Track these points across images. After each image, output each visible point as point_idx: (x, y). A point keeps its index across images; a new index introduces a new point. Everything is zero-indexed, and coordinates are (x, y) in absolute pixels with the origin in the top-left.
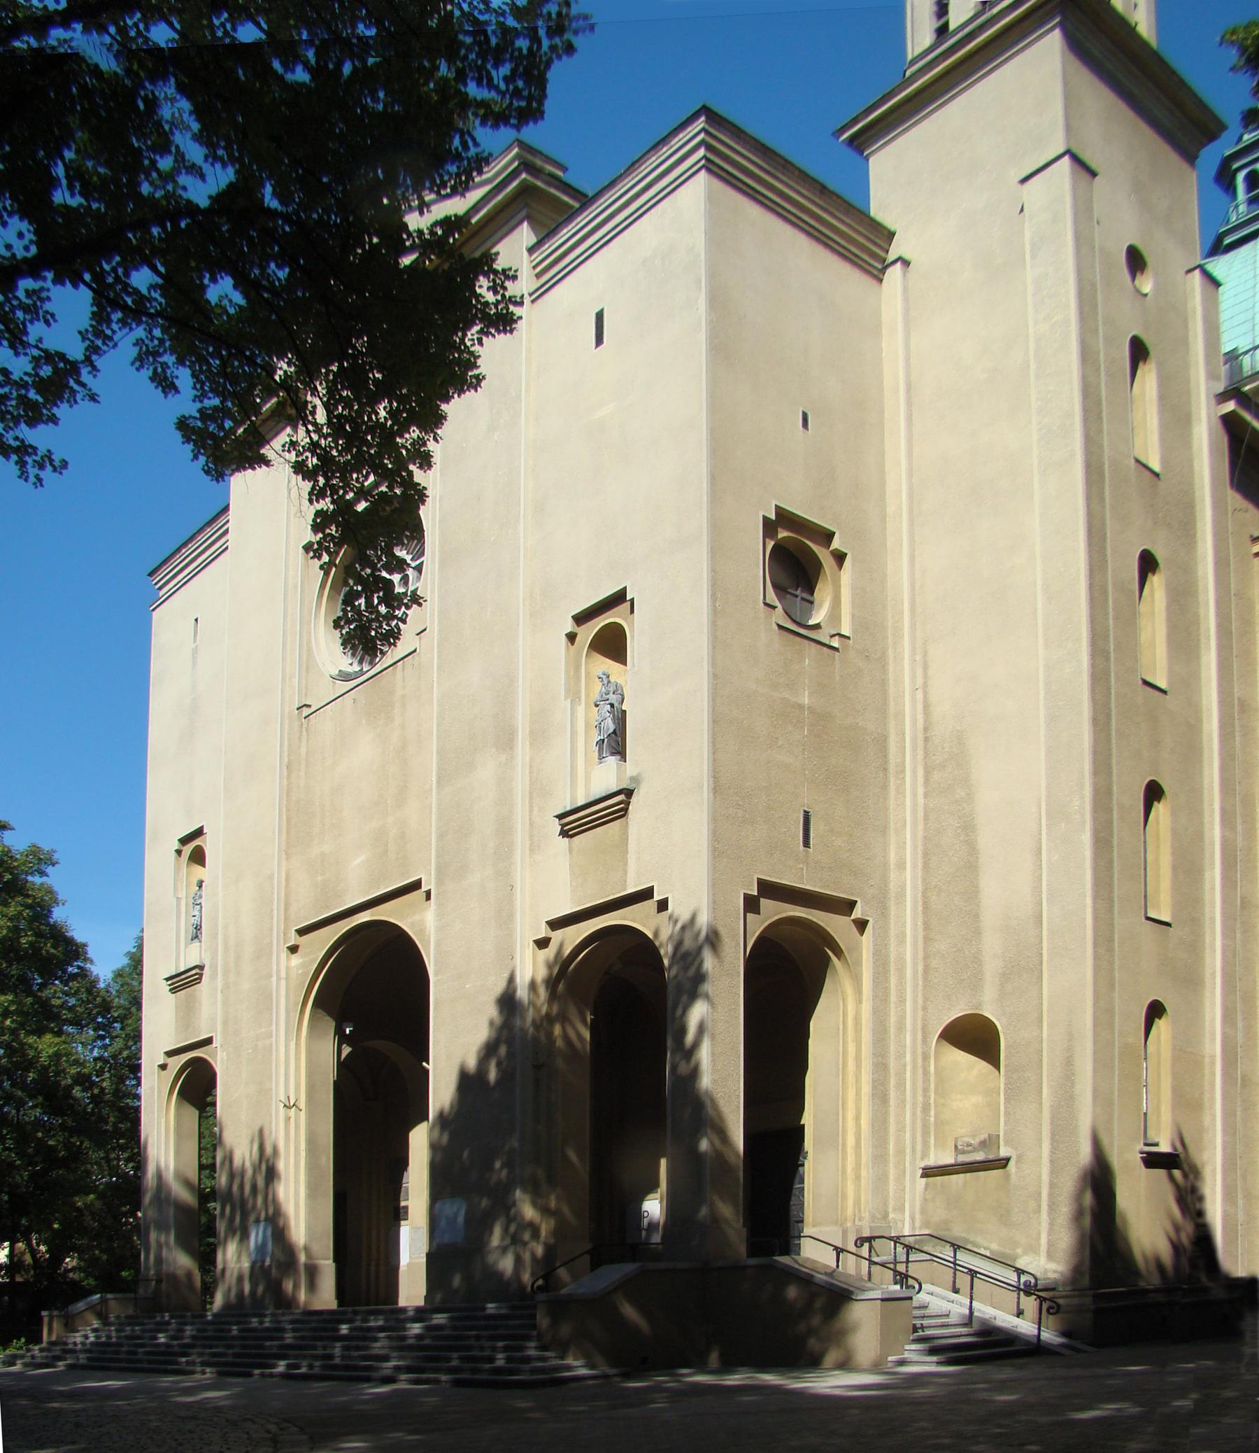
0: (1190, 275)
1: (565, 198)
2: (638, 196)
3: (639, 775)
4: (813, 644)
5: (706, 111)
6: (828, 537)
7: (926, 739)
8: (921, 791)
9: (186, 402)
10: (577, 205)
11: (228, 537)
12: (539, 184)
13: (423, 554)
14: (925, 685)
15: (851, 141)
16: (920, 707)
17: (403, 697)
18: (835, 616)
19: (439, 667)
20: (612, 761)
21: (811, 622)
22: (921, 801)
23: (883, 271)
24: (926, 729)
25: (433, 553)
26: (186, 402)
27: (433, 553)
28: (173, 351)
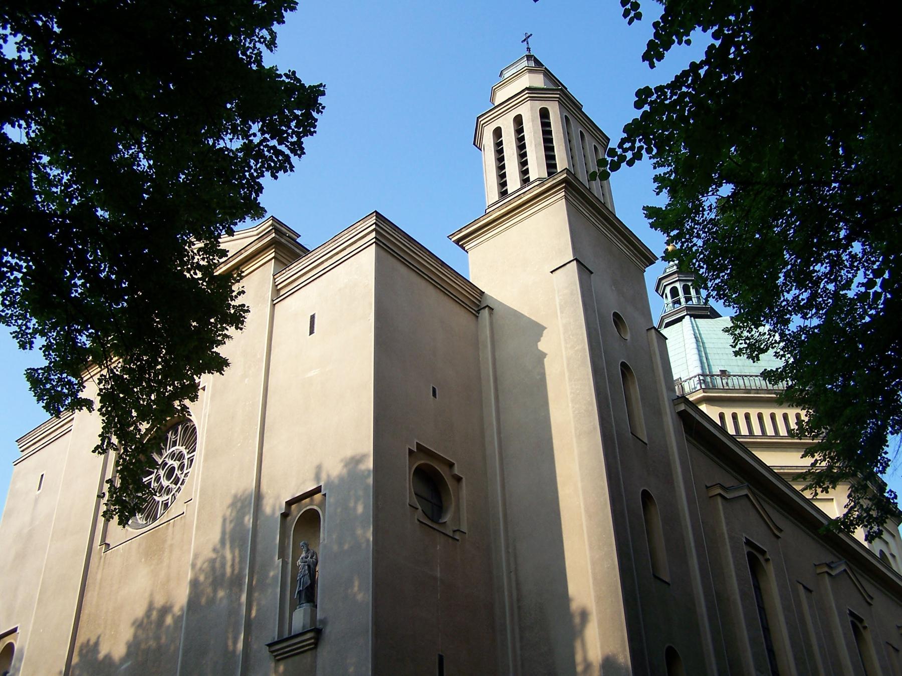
0: (649, 332)
1: (298, 251)
2: (337, 253)
3: (325, 618)
4: (442, 535)
5: (377, 214)
6: (451, 465)
7: (519, 608)
8: (518, 645)
9: (37, 359)
10: (279, 280)
11: (73, 423)
12: (283, 241)
13: (194, 451)
14: (516, 570)
15: (457, 242)
16: (514, 585)
17: (171, 545)
18: (457, 518)
19: (198, 528)
20: (306, 606)
21: (441, 521)
22: (519, 652)
23: (478, 312)
24: (518, 600)
25: (201, 451)
26: (37, 359)
27: (201, 451)
28: (272, 138)
